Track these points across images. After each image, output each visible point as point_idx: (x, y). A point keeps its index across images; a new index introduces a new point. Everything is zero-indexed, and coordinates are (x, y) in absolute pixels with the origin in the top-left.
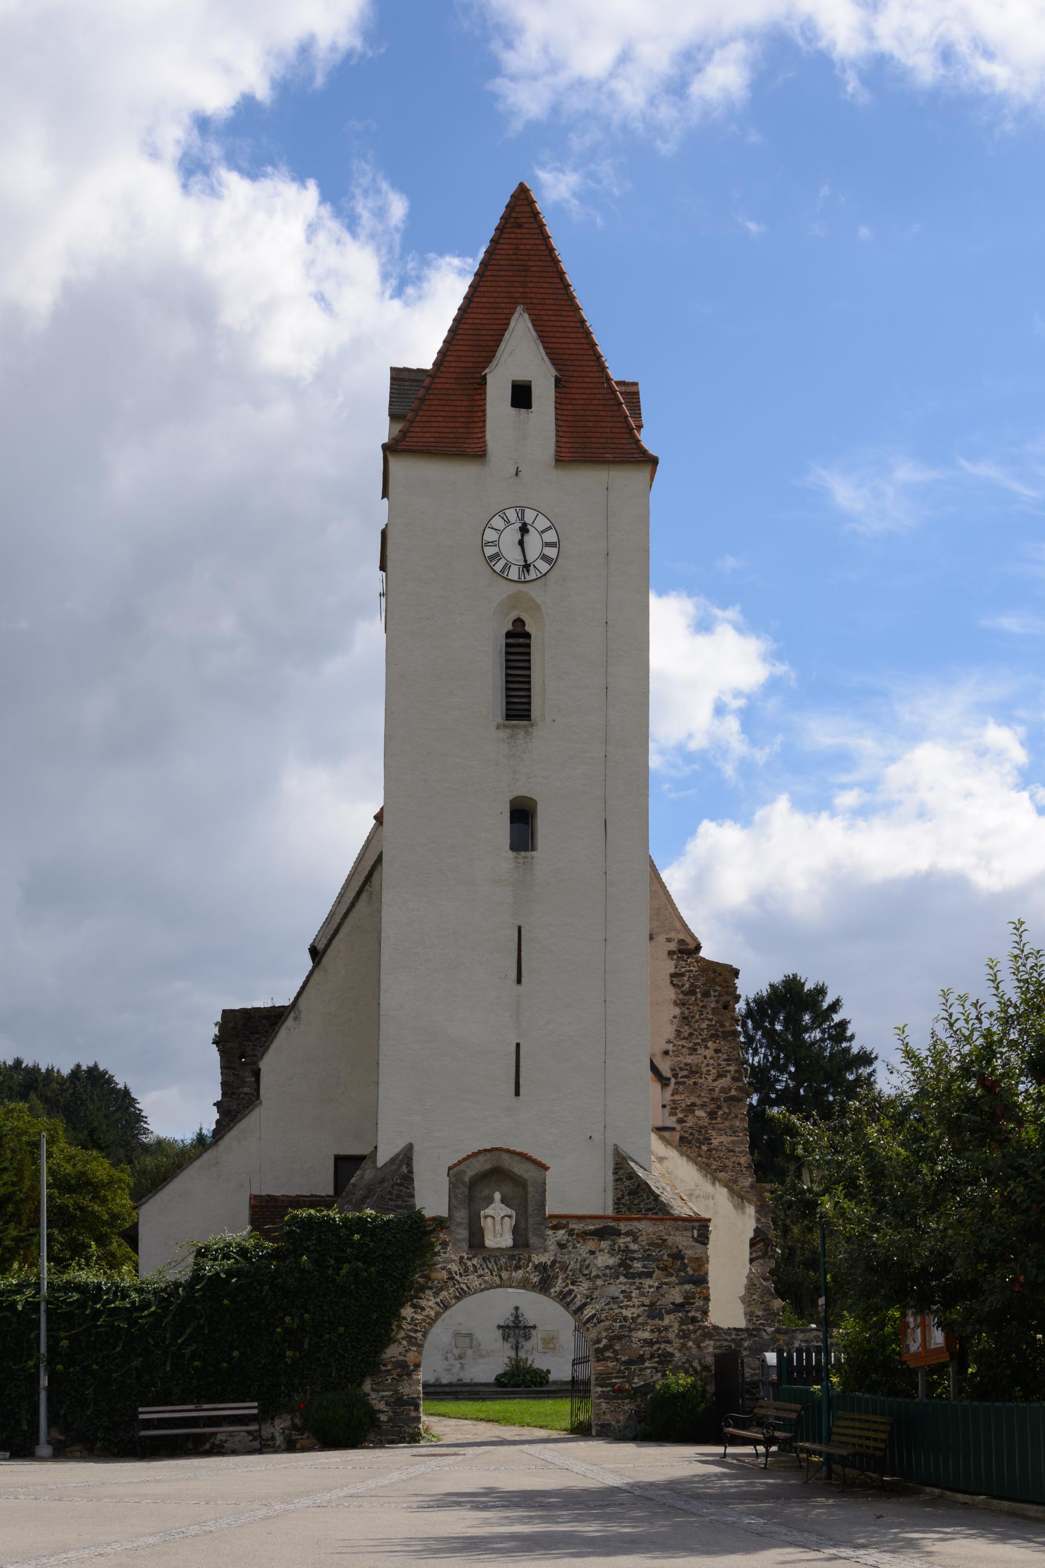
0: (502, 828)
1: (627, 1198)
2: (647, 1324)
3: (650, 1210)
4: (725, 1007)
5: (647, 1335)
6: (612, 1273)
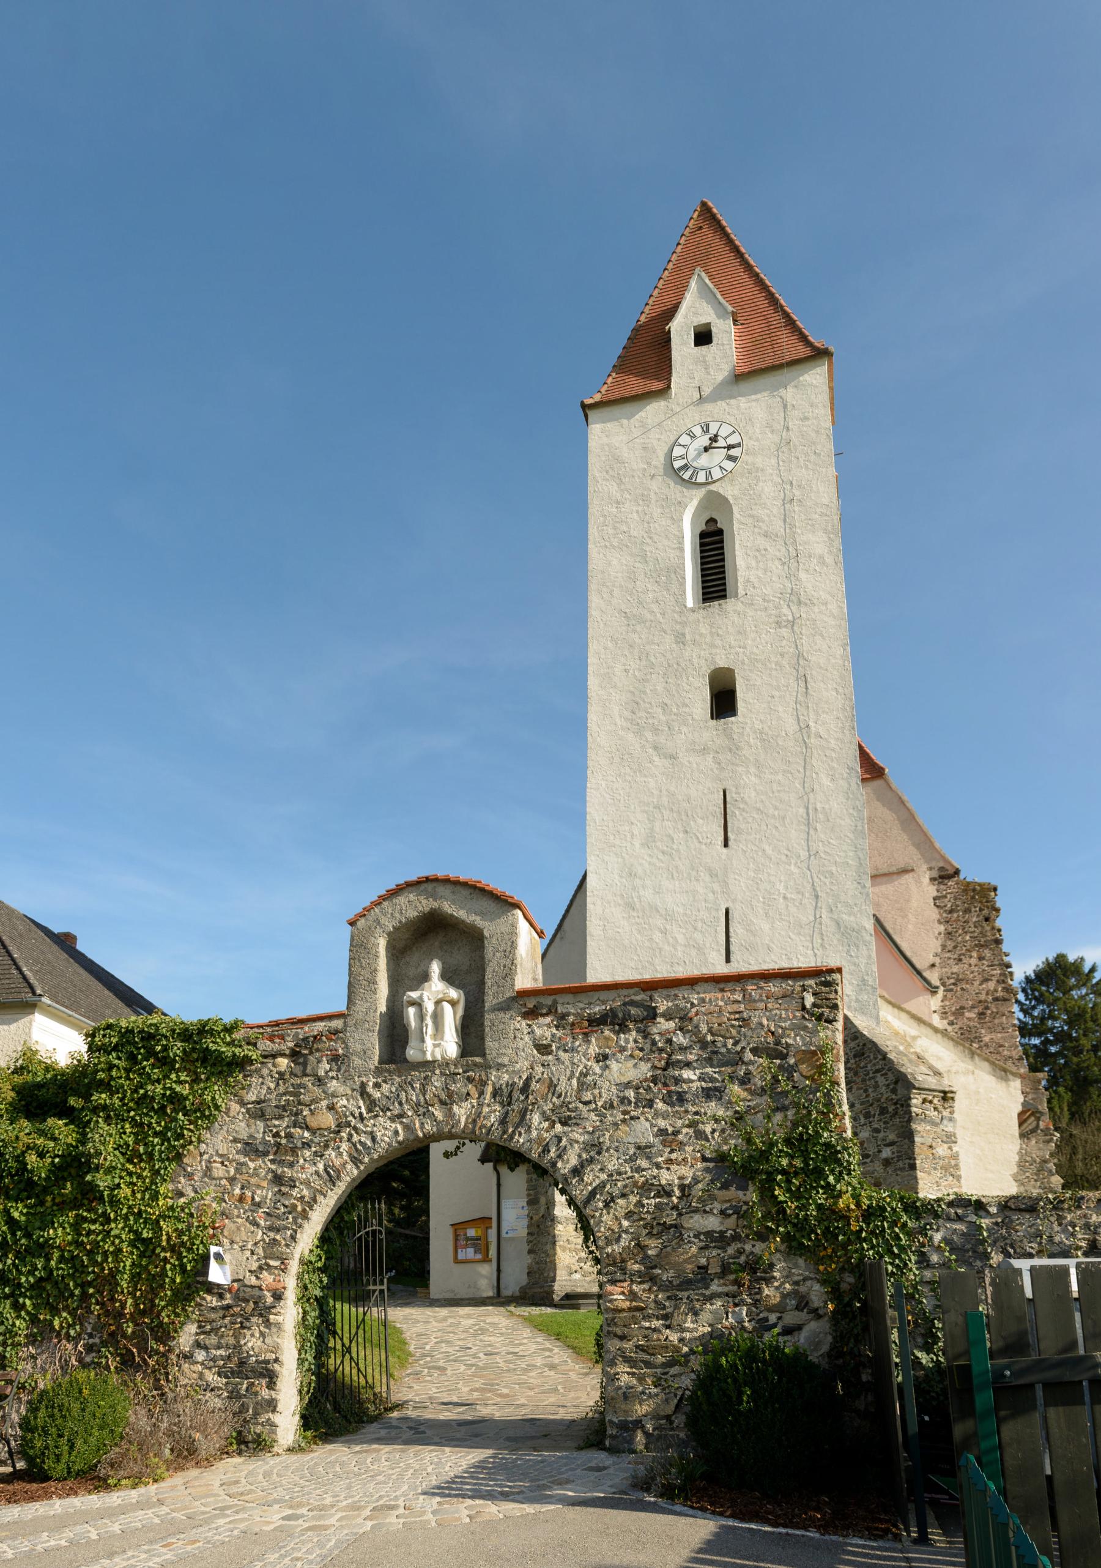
0: (701, 700)
1: (852, 1061)
2: (713, 1198)
3: (878, 1071)
4: (987, 919)
5: (712, 1223)
6: (636, 1099)
